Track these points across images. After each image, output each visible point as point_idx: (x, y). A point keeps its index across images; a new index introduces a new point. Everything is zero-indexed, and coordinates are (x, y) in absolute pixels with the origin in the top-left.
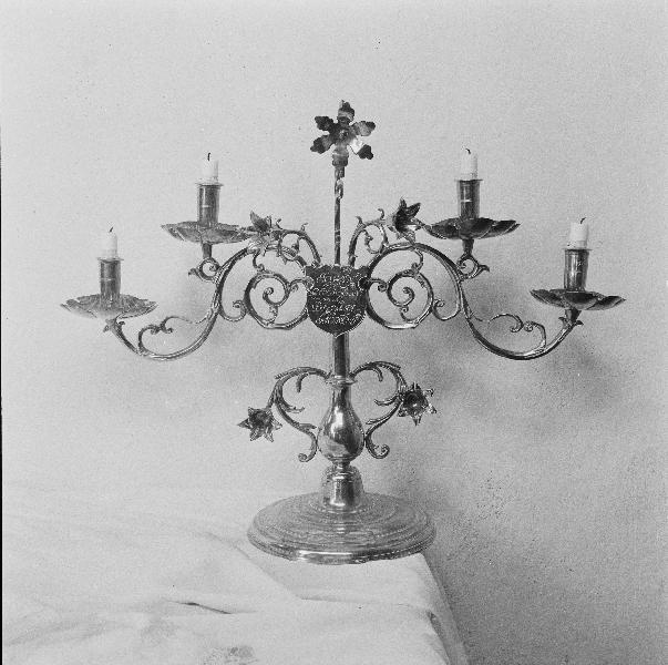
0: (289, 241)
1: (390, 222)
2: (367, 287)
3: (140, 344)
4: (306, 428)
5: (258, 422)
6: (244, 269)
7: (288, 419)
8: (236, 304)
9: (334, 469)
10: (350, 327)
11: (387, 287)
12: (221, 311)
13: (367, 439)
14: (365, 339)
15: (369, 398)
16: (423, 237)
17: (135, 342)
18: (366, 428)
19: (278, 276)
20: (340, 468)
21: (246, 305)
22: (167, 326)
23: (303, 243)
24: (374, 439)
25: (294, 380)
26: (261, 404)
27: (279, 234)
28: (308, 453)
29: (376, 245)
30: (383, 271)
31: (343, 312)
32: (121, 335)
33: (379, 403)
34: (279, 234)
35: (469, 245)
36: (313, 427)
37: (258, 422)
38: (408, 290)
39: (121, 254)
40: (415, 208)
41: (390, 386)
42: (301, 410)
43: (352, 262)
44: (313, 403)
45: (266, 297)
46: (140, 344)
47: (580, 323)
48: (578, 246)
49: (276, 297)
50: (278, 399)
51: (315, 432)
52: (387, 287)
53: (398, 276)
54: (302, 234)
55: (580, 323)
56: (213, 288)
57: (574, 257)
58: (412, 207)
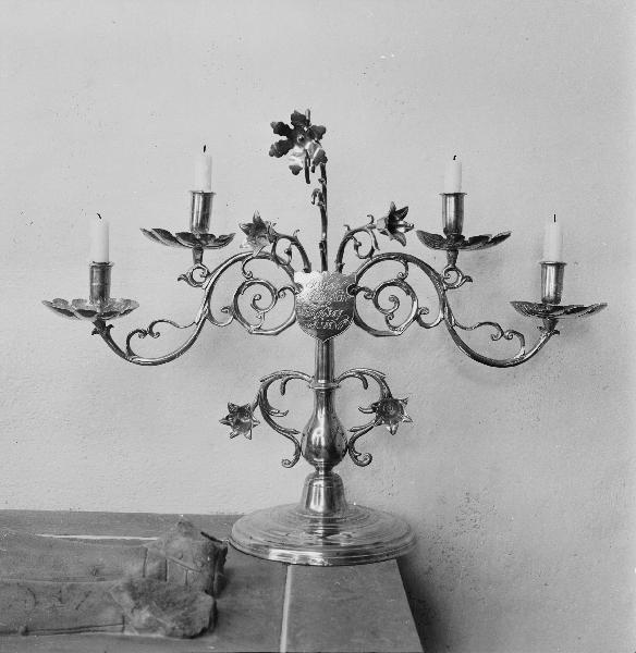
0: (283, 245)
1: (382, 225)
2: (355, 293)
3: (128, 348)
4: (289, 434)
5: (238, 418)
6: (234, 277)
7: (267, 418)
8: (225, 309)
9: (316, 475)
10: (337, 332)
11: (373, 296)
12: (209, 316)
13: (350, 447)
14: (353, 350)
15: (354, 406)
16: (415, 247)
17: (124, 350)
18: (349, 435)
19: (267, 285)
20: (322, 473)
21: (235, 311)
22: (155, 330)
23: (295, 250)
24: (358, 445)
25: (278, 383)
26: (247, 398)
27: (275, 238)
28: (292, 458)
29: (364, 251)
30: (370, 280)
31: (330, 318)
32: (108, 338)
33: (366, 386)
34: (275, 238)
35: (453, 260)
36: (296, 432)
37: (238, 418)
38: (396, 300)
39: (111, 260)
40: (403, 212)
41: (374, 395)
42: (285, 414)
43: (340, 269)
44: (299, 407)
45: (254, 306)
46: (128, 348)
47: (557, 332)
48: (554, 260)
49: (264, 303)
50: (262, 401)
51: (298, 437)
52: (373, 296)
53: (385, 285)
54: (294, 240)
55: (557, 332)
56: (201, 293)
57: (551, 271)
58: (402, 211)
